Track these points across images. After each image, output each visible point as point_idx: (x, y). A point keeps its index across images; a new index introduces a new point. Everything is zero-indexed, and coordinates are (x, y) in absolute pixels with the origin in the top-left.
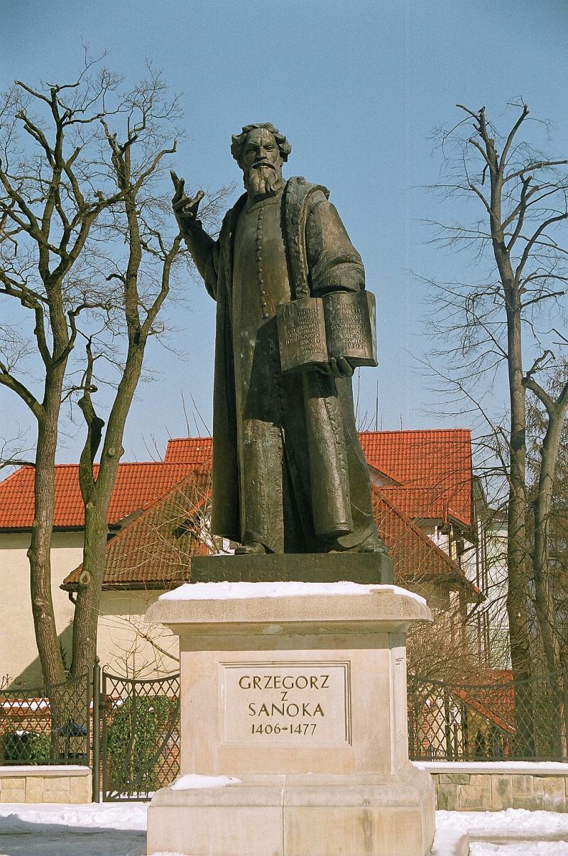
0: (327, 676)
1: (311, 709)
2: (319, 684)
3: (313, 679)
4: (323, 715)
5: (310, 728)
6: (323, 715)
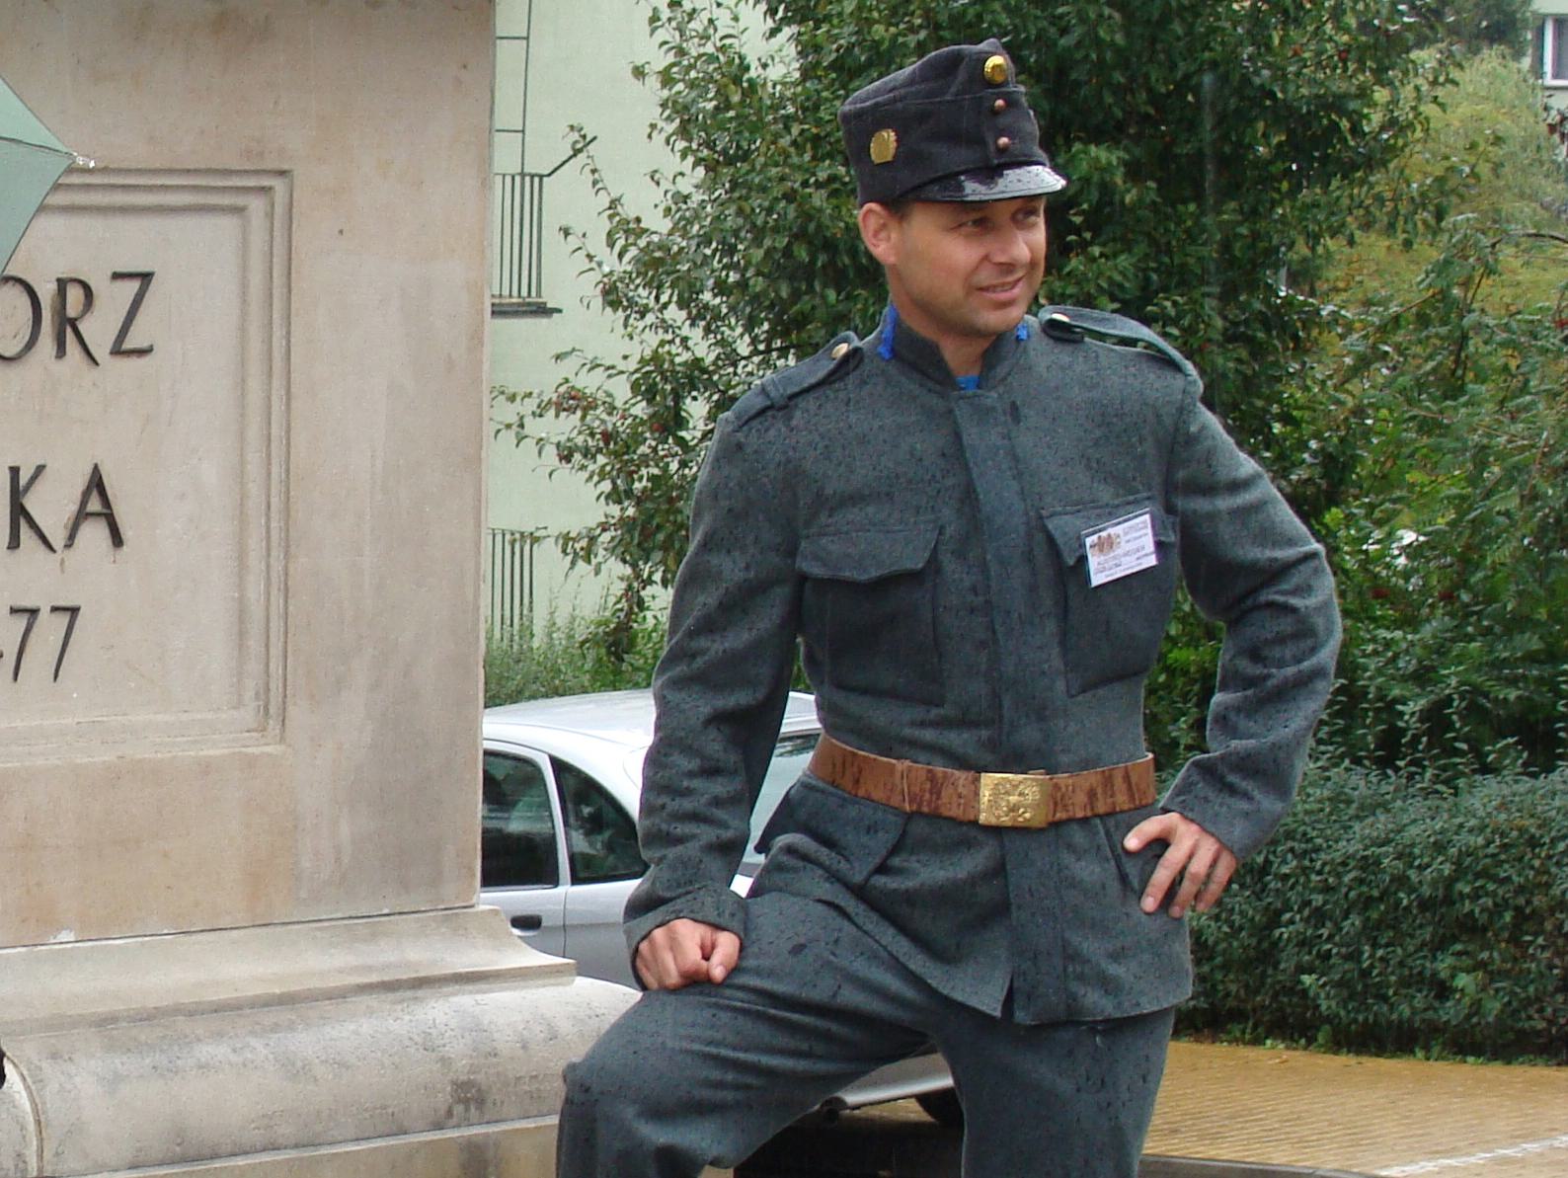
0: (146, 277)
1: (52, 506)
2: (99, 329)
3: (74, 295)
4: (117, 539)
5: (49, 629)
6: (117, 539)
